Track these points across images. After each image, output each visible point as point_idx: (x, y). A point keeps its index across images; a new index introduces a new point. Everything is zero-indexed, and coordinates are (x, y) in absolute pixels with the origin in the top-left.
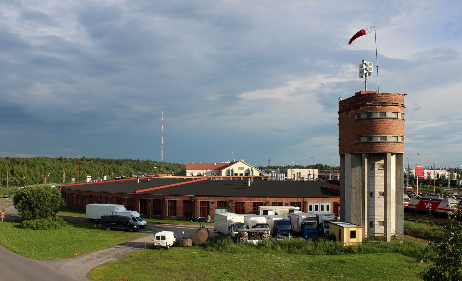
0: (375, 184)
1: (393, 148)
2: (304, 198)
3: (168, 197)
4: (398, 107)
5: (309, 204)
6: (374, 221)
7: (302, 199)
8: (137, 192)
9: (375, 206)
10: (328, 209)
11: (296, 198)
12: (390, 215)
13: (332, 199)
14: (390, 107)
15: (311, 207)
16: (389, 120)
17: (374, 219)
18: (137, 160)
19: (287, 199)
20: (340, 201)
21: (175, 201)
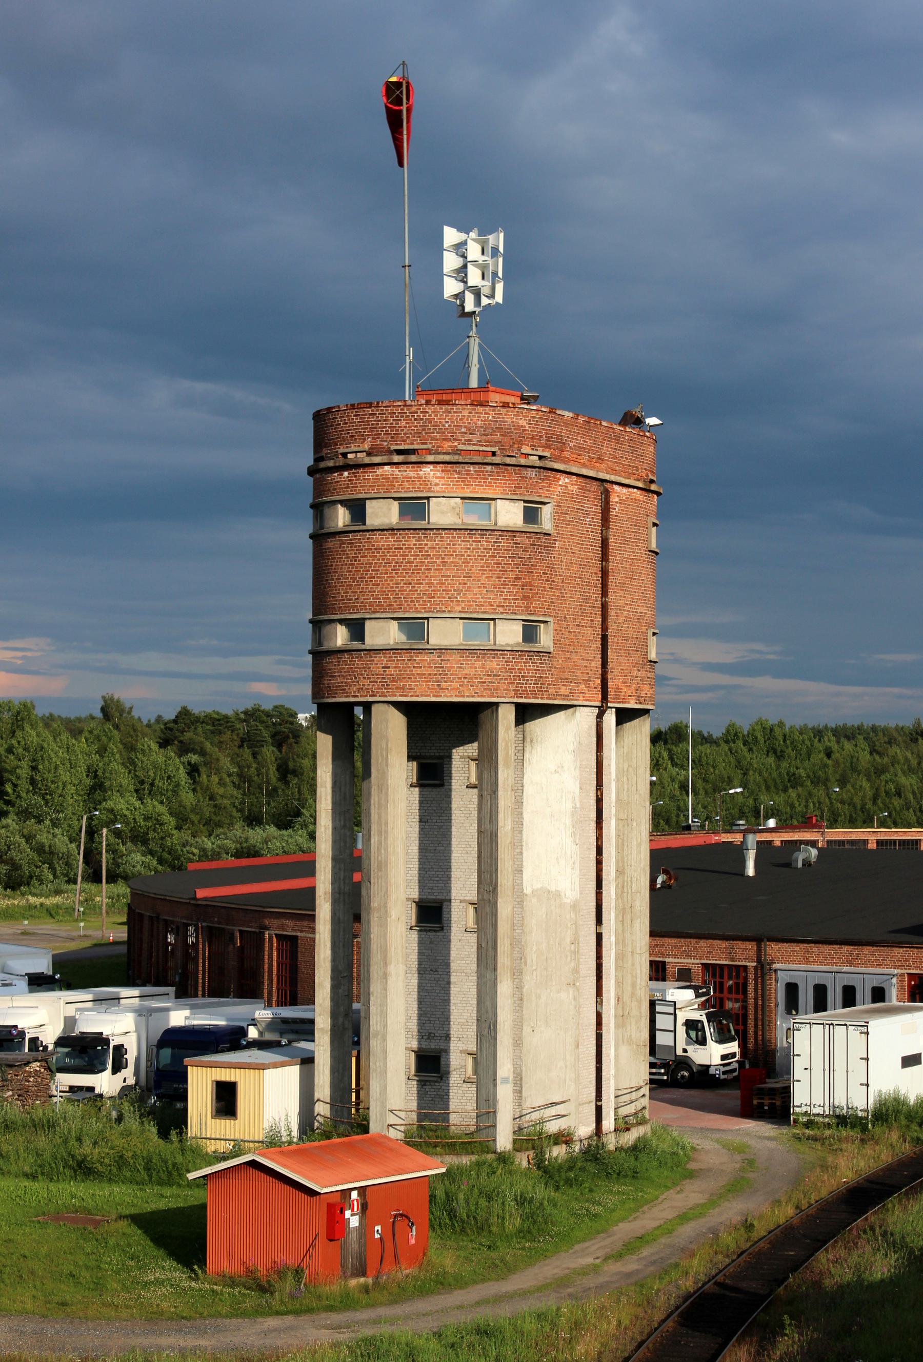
0: (448, 860)
1: (400, 678)
2: (758, 940)
3: (276, 922)
4: (427, 469)
5: (784, 978)
6: (447, 1051)
7: (751, 947)
8: (201, 893)
9: (448, 974)
10: (792, 989)
11: (724, 944)
12: (384, 1015)
13: (899, 952)
14: (380, 471)
15: (792, 989)
16: (376, 537)
17: (447, 1037)
18: (47, 715)
19: (683, 943)
20: (175, 939)
21: (664, 963)
